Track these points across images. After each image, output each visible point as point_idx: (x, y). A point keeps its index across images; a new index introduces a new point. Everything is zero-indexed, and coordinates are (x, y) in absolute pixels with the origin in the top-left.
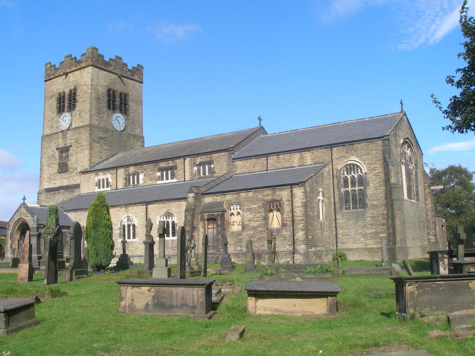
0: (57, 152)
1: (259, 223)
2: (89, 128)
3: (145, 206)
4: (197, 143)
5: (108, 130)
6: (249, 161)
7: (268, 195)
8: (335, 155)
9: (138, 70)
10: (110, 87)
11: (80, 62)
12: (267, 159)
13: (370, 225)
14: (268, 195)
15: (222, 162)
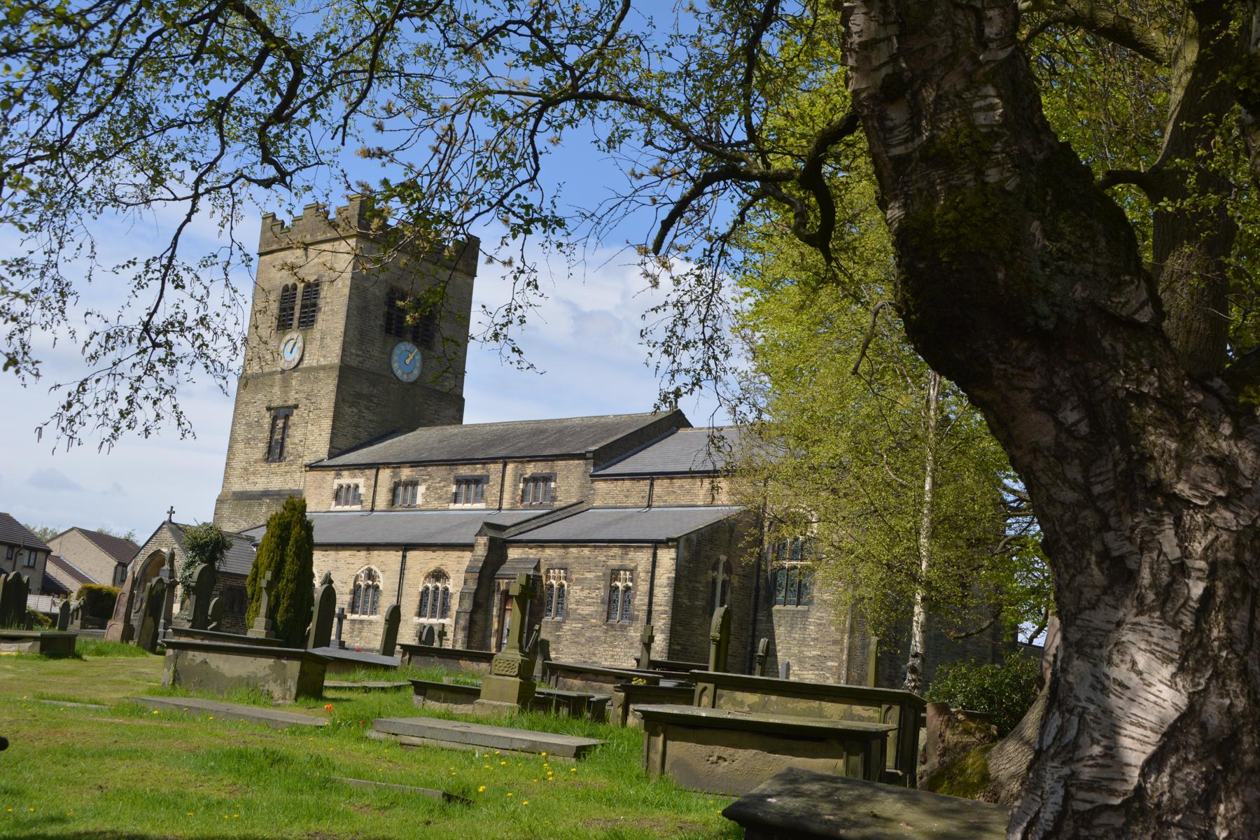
0: (268, 415)
1: (592, 608)
3: (650, 551)
4: (543, 431)
5: (384, 376)
6: (620, 483)
7: (614, 557)
10: (395, 284)
12: (652, 485)
13: (814, 640)
14: (614, 557)
15: (571, 479)
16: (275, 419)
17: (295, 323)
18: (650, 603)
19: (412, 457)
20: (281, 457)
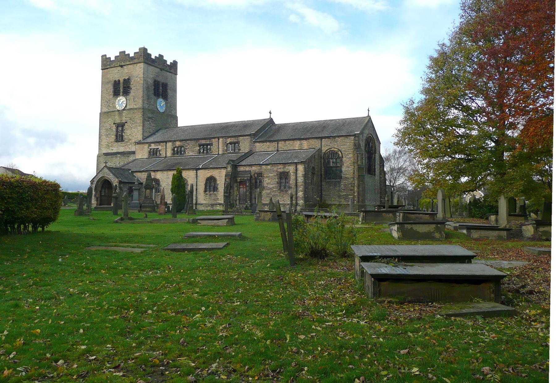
0: (114, 126)
2: (142, 110)
5: (155, 111)
7: (280, 168)
8: (323, 144)
9: (174, 64)
11: (132, 58)
14: (280, 168)
16: (117, 127)
17: (121, 94)
18: (296, 182)
19: (182, 138)
20: (122, 140)
